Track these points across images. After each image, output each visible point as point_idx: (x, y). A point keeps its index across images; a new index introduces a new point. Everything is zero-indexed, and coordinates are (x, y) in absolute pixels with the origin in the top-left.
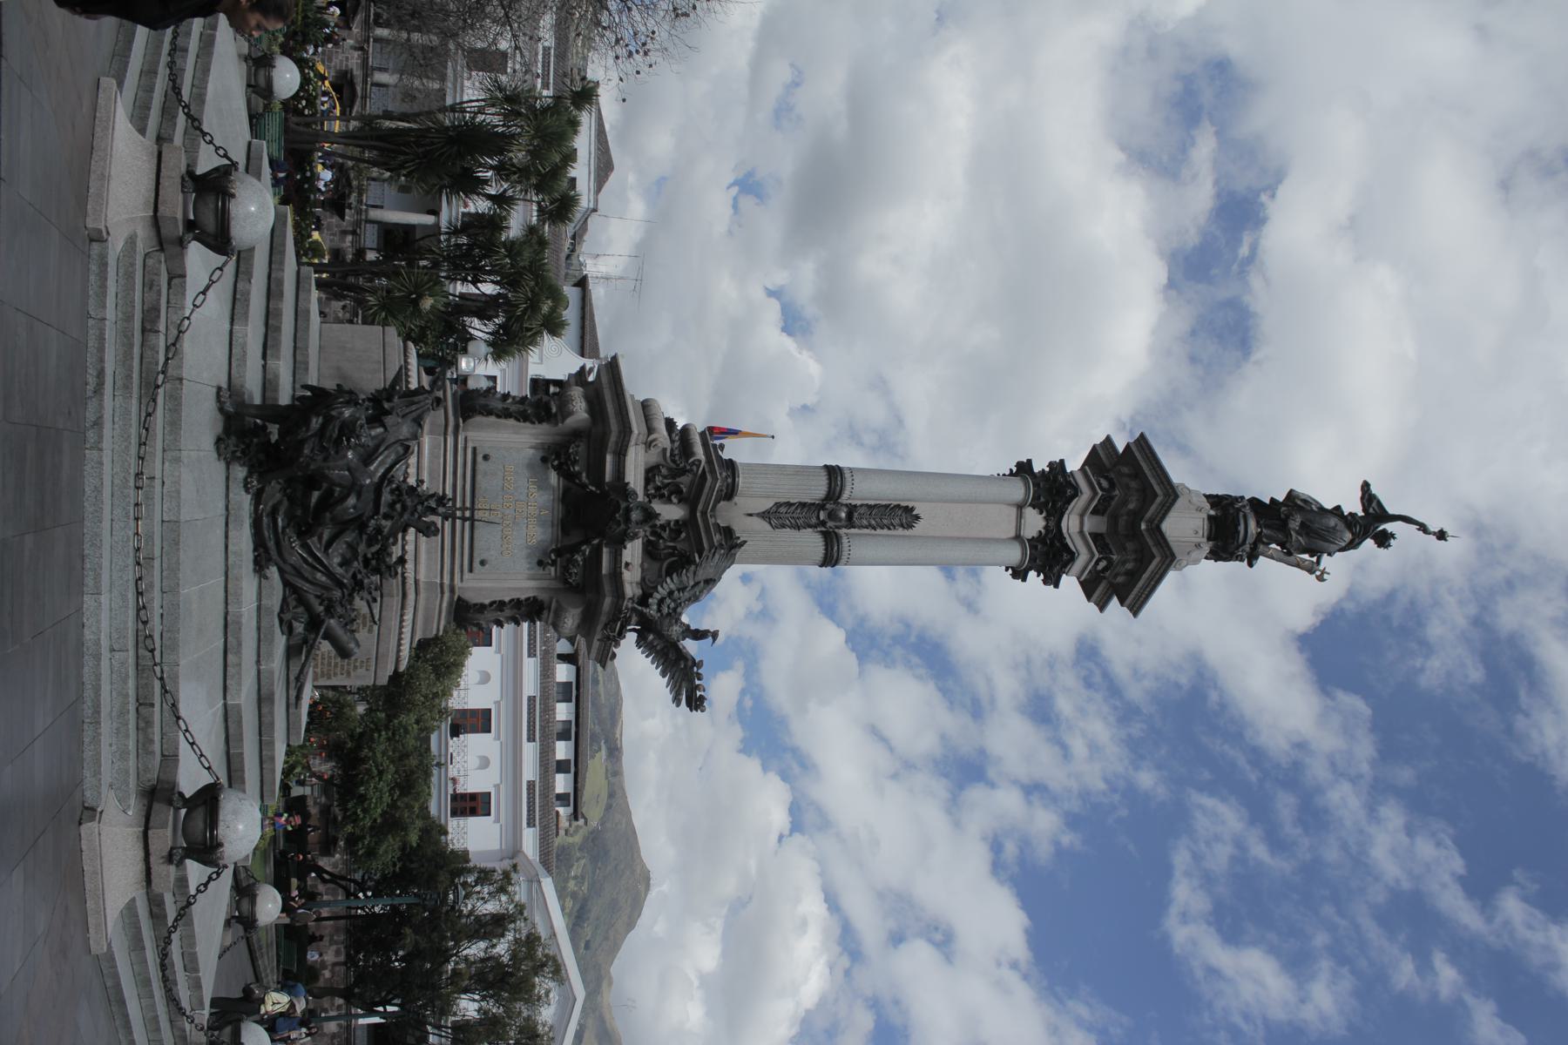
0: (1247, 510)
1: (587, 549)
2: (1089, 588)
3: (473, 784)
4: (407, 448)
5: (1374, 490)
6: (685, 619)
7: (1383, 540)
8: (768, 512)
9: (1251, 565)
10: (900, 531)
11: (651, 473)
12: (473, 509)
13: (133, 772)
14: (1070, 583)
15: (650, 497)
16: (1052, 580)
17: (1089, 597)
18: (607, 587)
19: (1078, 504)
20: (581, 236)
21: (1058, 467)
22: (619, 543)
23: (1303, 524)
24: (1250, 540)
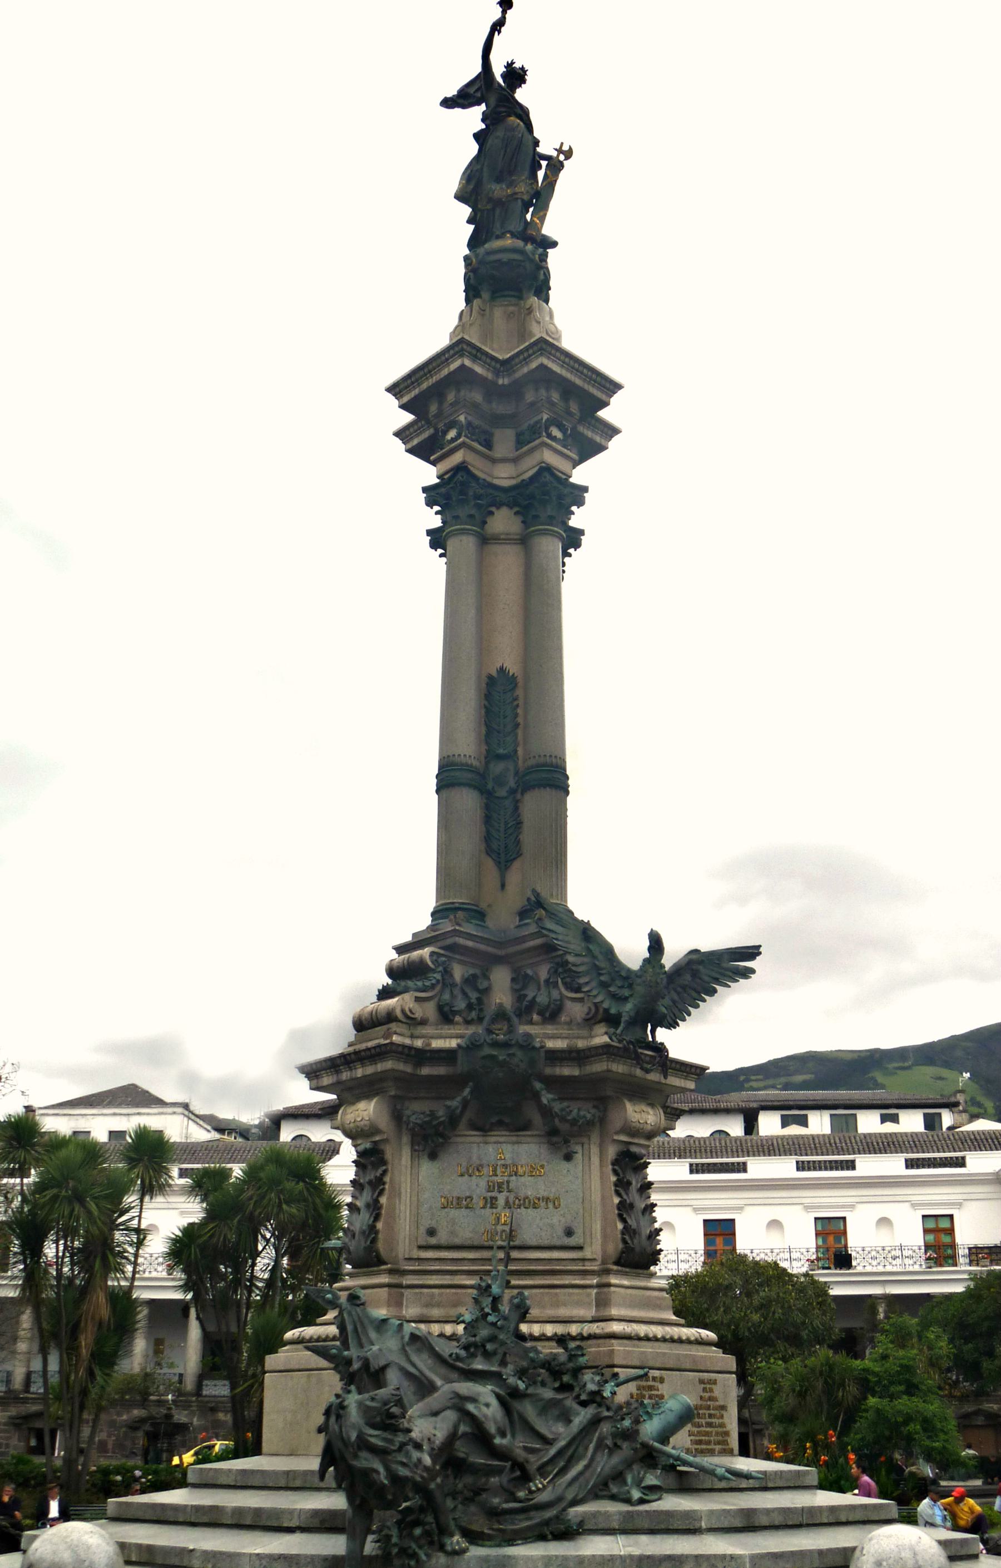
0: (481, 251)
1: (546, 1098)
2: (589, 450)
3: (912, 1235)
4: (414, 1337)
5: (452, 92)
7: (516, 76)
8: (498, 864)
9: (554, 244)
10: (519, 692)
14: (579, 475)
15: (480, 1019)
16: (578, 495)
17: (601, 448)
19: (479, 467)
21: (432, 495)
23: (499, 180)
24: (520, 243)
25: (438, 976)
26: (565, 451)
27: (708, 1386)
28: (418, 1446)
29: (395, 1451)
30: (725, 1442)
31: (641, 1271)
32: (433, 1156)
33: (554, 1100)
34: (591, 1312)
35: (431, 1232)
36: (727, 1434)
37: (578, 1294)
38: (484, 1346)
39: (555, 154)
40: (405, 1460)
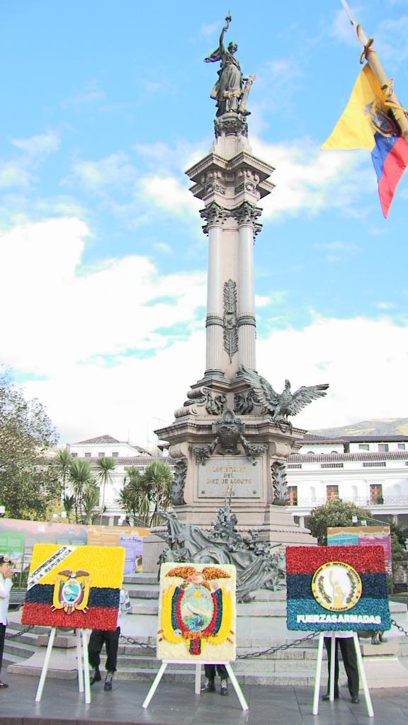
0: (221, 117)
2: (264, 193)
5: (208, 56)
6: (280, 393)
7: (232, 48)
13: (295, 662)
18: (264, 431)
20: (141, 449)
25: (206, 397)
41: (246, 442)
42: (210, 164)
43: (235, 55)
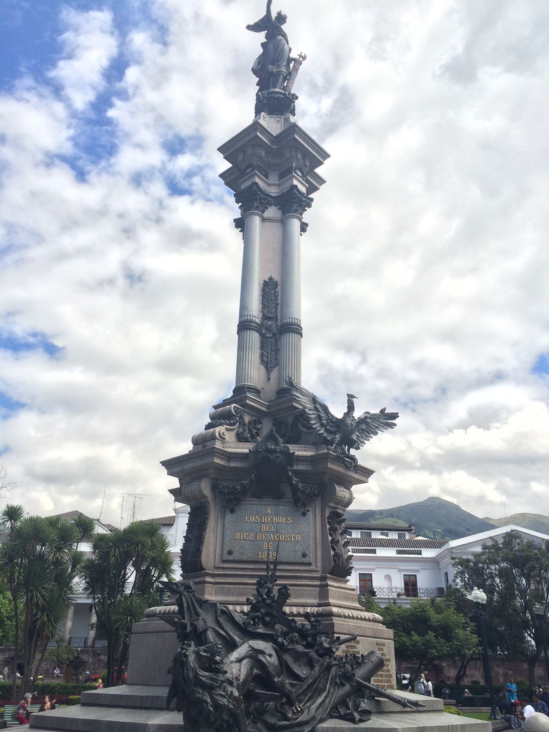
3: (399, 583)
5: (252, 23)
7: (281, 18)
11: (240, 438)
12: (266, 563)
22: (291, 458)
23: (273, 64)
25: (237, 419)
26: (303, 182)
27: (381, 647)
28: (231, 683)
29: (217, 687)
30: (390, 681)
31: (342, 579)
32: (232, 511)
33: (299, 482)
34: (315, 601)
35: (230, 553)
36: (391, 676)
37: (309, 590)
38: (263, 618)
39: (298, 57)
40: (224, 694)
41: (295, 480)
42: (251, 137)
43: (283, 27)
